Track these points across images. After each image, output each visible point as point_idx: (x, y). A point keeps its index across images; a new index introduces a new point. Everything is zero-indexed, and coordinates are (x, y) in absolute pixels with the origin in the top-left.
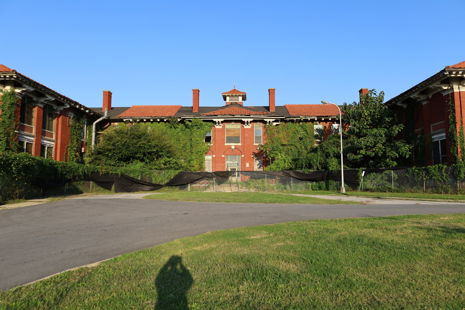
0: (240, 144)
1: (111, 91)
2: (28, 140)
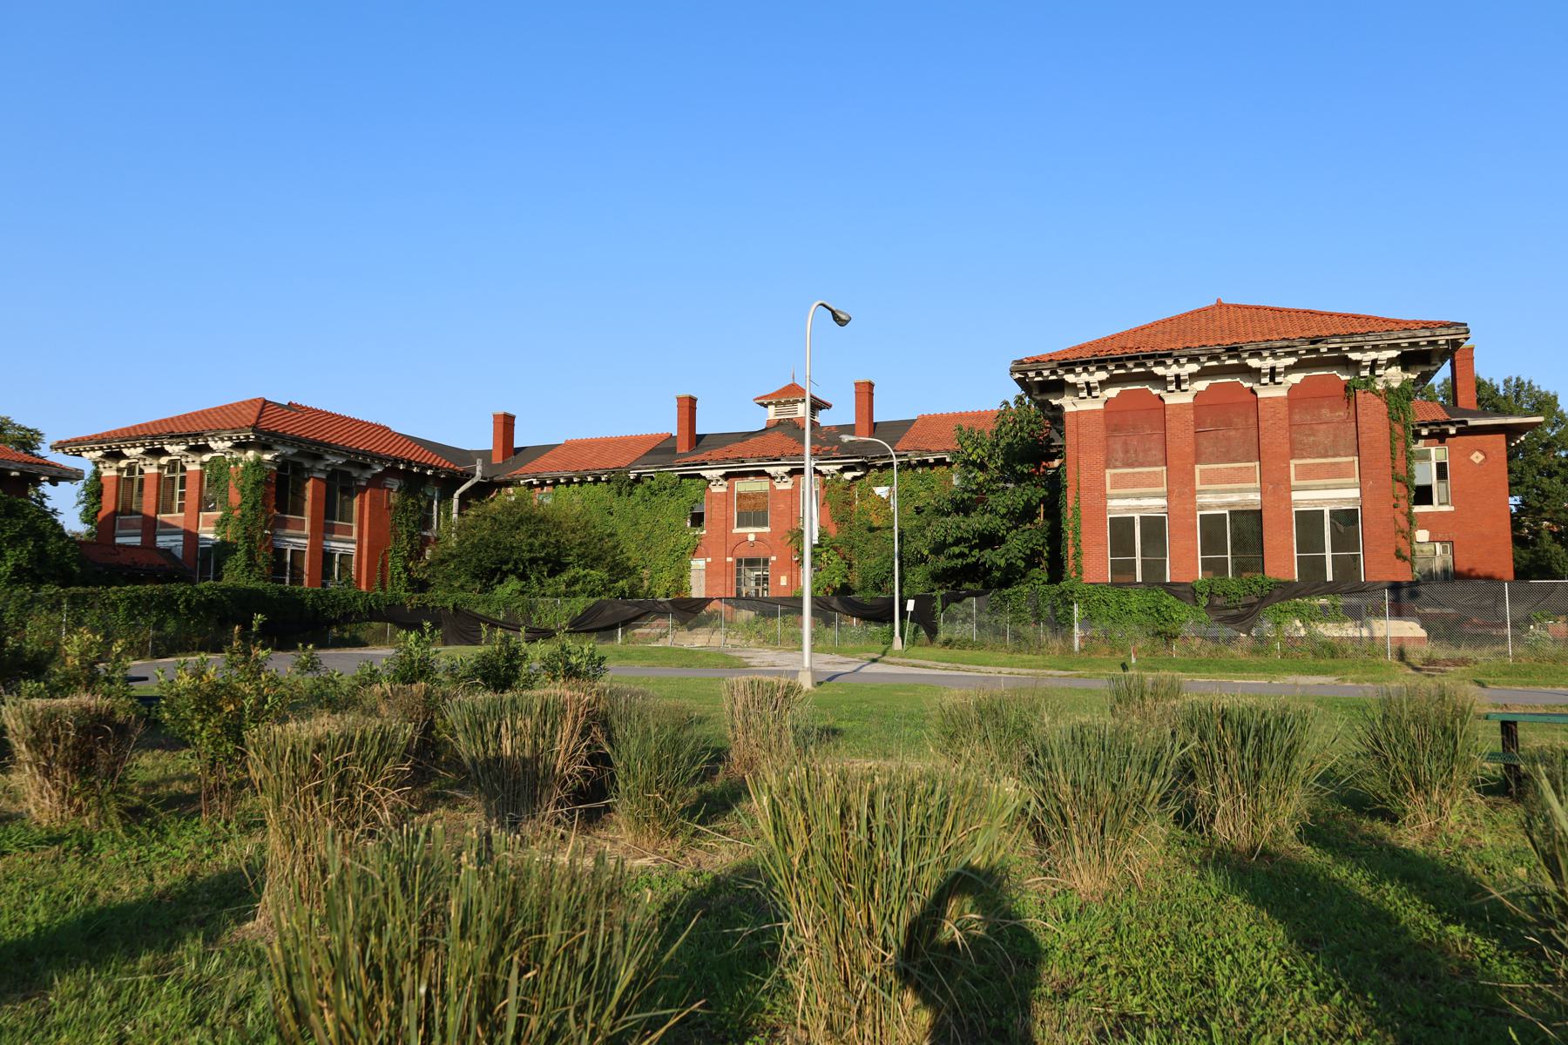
0: (767, 529)
1: (511, 412)
2: (295, 544)
